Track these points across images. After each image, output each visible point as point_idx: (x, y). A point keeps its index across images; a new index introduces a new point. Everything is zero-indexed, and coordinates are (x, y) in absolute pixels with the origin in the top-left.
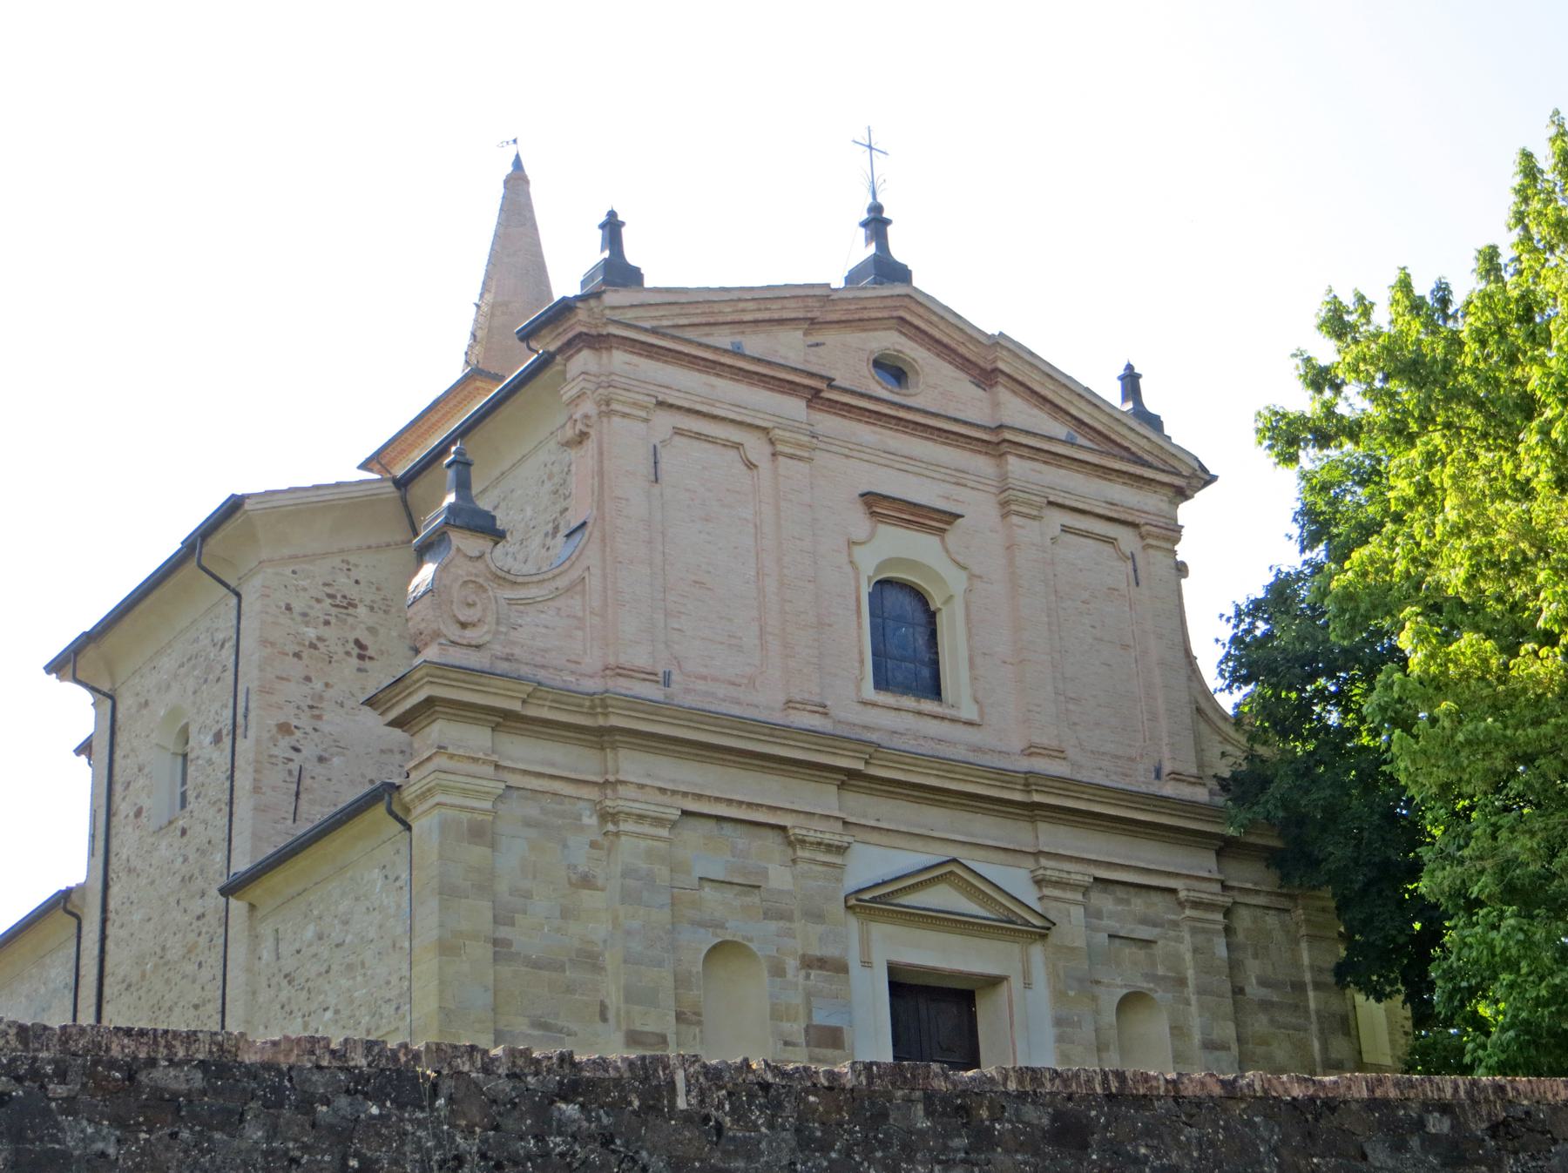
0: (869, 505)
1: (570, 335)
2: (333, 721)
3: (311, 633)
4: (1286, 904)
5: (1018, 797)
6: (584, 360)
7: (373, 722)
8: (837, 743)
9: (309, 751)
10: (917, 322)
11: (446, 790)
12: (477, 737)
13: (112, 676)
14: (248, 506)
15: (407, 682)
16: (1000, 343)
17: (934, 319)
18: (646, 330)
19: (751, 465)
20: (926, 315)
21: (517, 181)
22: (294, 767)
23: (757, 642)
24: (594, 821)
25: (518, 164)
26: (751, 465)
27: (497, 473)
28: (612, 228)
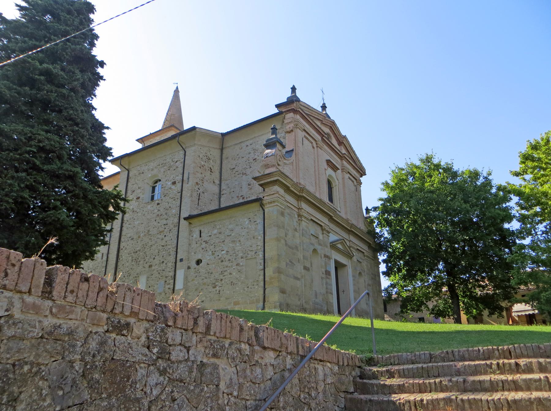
2: (206, 184)
3: (203, 163)
6: (291, 115)
7: (256, 184)
9: (201, 190)
11: (278, 202)
12: (282, 191)
13: (129, 166)
14: (197, 130)
16: (345, 137)
18: (305, 113)
19: (313, 148)
21: (177, 91)
22: (198, 193)
24: (296, 216)
25: (177, 88)
26: (313, 148)
27: (253, 137)
28: (294, 89)
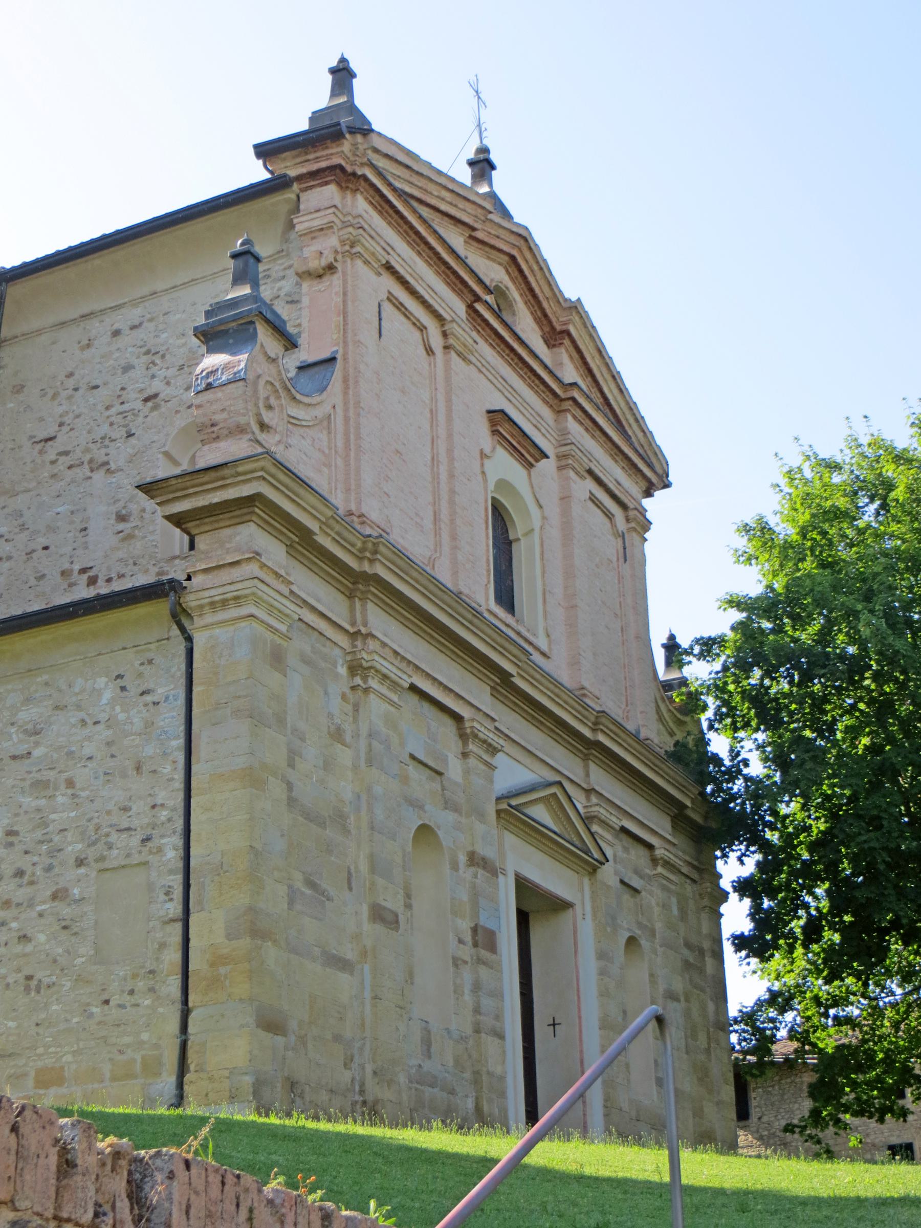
0: (493, 423)
1: (323, 164)
4: (695, 876)
5: (587, 733)
6: (329, 193)
8: (507, 645)
10: (524, 267)
12: (275, 552)
15: (226, 472)
17: (535, 268)
18: (395, 190)
20: (531, 261)
23: (432, 526)
26: (429, 351)
